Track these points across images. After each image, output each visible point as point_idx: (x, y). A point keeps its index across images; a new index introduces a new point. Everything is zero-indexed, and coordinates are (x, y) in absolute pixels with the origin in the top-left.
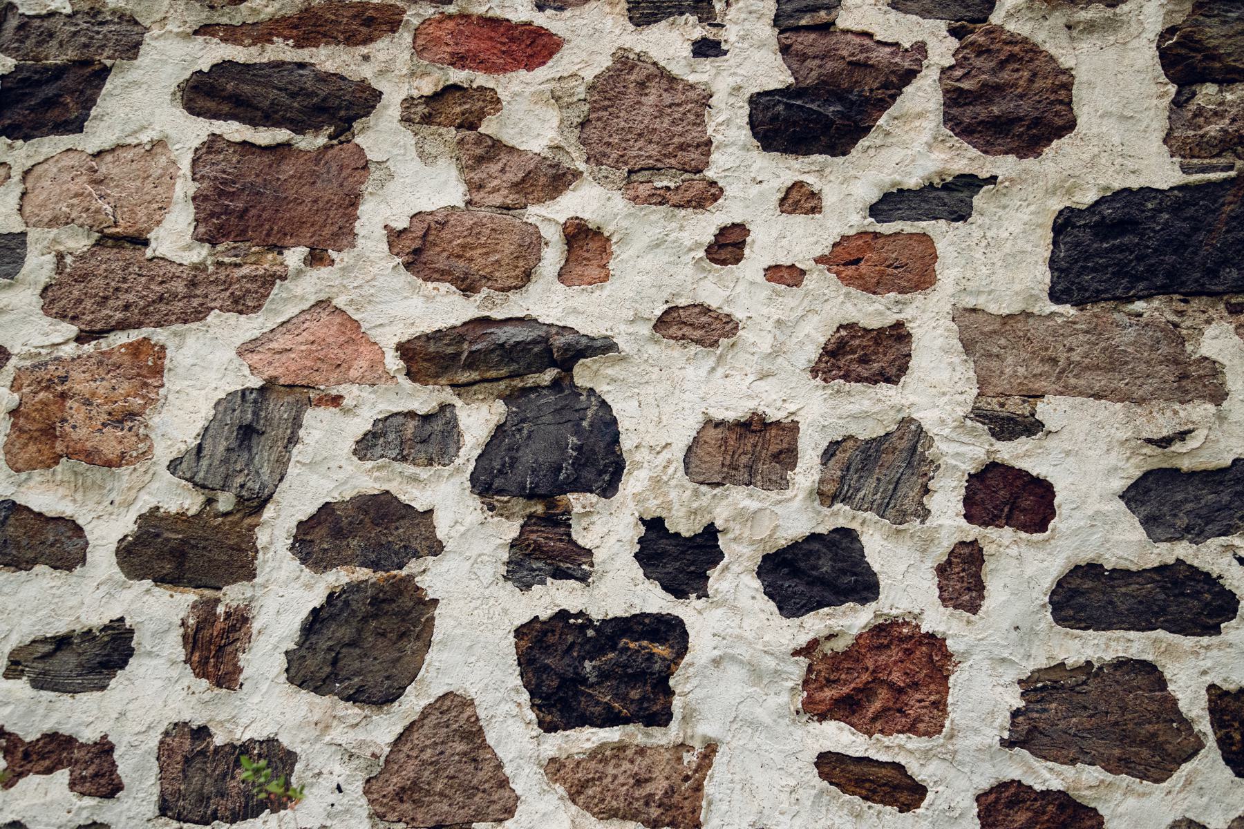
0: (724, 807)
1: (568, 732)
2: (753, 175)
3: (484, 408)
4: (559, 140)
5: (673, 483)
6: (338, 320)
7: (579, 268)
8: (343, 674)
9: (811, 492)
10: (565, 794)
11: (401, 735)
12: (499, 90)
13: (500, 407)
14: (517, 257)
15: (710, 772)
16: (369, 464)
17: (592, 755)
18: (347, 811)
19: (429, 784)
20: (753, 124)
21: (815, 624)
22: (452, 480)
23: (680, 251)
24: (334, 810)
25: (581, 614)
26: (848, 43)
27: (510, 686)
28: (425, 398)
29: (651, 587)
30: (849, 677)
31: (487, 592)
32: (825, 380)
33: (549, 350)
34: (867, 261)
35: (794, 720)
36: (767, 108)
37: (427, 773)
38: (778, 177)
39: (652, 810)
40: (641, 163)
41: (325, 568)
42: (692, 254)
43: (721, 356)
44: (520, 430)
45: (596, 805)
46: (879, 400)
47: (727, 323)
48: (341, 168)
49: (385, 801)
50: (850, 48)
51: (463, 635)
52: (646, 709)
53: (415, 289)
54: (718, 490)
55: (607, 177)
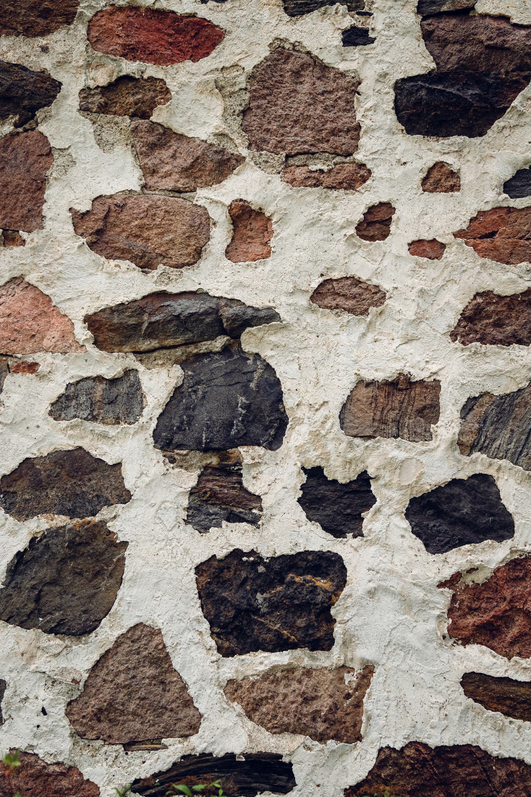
0: (382, 722)
1: (243, 657)
2: (398, 157)
3: (164, 372)
4: (223, 128)
5: (330, 436)
6: (31, 295)
7: (244, 246)
8: (45, 609)
9: (452, 443)
10: (242, 711)
11: (98, 662)
12: (168, 81)
13: (177, 371)
14: (189, 237)
15: (368, 691)
16: (64, 424)
17: (265, 676)
18: (52, 731)
19: (123, 705)
20: (398, 109)
21: (457, 559)
22: (137, 437)
23: (333, 229)
24: (40, 731)
25: (252, 553)
26: (486, 28)
27: (193, 617)
28: (111, 364)
29: (313, 528)
30: (489, 606)
31: (170, 535)
32: (463, 343)
33: (219, 320)
34: (501, 234)
35: (441, 644)
36: (411, 93)
37: (121, 695)
38: (421, 158)
39: (318, 725)
40: (298, 148)
41: (27, 516)
42: (344, 232)
43: (370, 323)
44: (195, 392)
45: (270, 721)
46: (512, 360)
47: (376, 293)
48: (27, 154)
49: (85, 721)
50: (488, 32)
51: (150, 573)
52: (311, 635)
53: (100, 267)
54: (369, 443)
55: (267, 162)
